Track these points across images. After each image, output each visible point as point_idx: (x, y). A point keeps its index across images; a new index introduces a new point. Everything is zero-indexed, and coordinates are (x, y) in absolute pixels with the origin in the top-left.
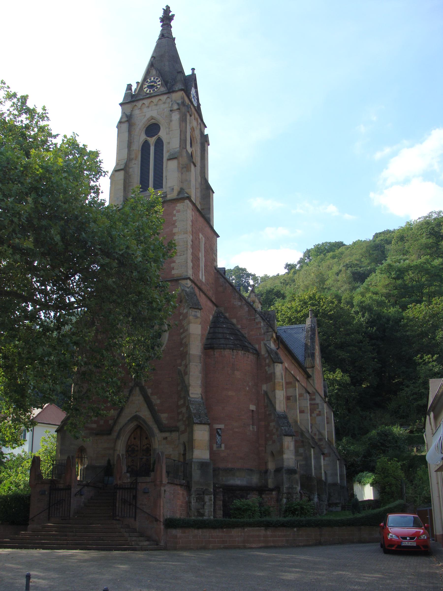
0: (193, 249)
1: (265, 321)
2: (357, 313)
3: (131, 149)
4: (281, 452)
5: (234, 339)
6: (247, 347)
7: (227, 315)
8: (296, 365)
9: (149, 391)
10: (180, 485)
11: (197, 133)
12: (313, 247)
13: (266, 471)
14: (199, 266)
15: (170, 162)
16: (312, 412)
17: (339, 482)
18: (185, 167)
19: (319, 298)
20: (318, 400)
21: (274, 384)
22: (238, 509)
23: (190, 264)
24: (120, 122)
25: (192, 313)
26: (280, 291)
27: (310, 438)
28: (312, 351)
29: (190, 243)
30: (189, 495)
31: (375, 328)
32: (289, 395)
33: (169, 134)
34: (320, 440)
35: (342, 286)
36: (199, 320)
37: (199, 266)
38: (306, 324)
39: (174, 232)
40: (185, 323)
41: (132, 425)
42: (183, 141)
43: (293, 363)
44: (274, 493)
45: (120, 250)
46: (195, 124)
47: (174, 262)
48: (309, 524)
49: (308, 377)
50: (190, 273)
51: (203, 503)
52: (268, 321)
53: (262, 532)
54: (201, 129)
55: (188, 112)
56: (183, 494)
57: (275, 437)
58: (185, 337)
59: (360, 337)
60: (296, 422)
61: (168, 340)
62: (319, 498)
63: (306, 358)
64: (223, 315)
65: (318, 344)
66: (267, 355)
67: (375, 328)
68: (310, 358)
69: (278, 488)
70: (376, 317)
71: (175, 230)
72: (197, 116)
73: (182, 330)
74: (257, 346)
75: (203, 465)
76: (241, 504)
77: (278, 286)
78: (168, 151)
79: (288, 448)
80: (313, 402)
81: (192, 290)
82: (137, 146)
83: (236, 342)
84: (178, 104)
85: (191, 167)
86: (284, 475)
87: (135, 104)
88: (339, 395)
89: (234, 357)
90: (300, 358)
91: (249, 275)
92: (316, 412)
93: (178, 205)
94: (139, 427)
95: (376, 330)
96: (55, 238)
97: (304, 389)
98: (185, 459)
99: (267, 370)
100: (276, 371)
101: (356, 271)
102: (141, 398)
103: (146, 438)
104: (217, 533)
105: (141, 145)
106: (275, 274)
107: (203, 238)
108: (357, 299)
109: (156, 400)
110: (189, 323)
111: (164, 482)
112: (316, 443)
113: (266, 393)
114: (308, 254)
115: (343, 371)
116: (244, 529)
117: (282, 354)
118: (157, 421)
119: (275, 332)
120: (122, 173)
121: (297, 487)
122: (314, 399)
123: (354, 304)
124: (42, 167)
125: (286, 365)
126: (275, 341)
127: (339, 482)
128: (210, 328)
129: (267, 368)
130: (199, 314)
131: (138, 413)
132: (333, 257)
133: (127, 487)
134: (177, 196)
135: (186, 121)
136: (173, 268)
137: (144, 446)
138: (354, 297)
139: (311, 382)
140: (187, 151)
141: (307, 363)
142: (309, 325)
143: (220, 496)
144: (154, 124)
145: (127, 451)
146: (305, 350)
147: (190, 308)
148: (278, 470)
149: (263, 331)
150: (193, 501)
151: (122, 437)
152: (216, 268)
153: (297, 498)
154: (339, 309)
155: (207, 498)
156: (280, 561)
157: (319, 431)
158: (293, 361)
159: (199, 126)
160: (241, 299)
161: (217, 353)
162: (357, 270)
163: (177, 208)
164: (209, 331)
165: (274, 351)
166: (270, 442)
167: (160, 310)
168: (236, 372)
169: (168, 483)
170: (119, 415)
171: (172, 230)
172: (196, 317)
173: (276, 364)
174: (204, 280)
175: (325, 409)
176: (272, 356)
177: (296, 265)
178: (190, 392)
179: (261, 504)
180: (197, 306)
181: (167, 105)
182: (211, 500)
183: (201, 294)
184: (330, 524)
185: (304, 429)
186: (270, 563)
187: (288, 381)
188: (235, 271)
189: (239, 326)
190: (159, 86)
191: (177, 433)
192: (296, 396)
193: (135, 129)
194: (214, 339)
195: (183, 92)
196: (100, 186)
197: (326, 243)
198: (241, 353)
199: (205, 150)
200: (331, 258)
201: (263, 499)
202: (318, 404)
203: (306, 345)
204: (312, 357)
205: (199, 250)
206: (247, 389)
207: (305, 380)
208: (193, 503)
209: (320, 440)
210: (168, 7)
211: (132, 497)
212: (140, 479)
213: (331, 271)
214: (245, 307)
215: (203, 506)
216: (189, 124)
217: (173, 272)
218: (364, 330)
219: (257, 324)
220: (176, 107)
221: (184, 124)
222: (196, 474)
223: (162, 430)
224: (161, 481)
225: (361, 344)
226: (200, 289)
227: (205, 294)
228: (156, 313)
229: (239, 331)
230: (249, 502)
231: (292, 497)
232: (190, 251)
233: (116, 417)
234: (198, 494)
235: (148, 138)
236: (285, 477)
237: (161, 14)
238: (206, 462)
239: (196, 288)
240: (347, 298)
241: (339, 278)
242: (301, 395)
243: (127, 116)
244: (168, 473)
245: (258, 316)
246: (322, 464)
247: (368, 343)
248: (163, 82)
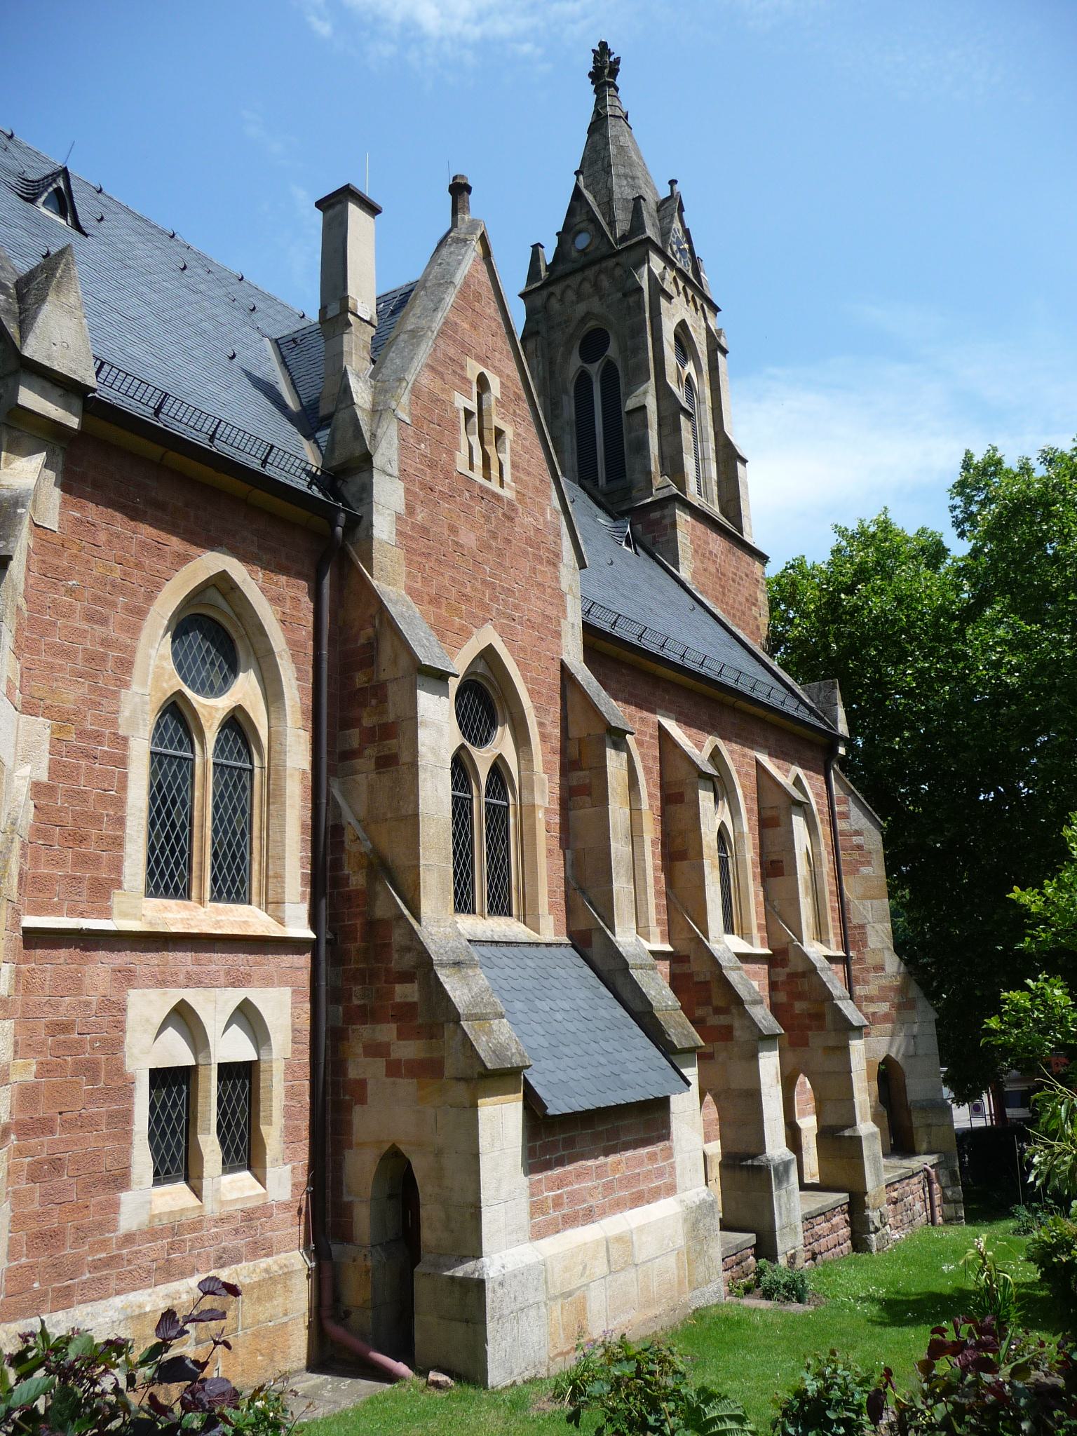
210: (603, 45)
235: (585, 365)
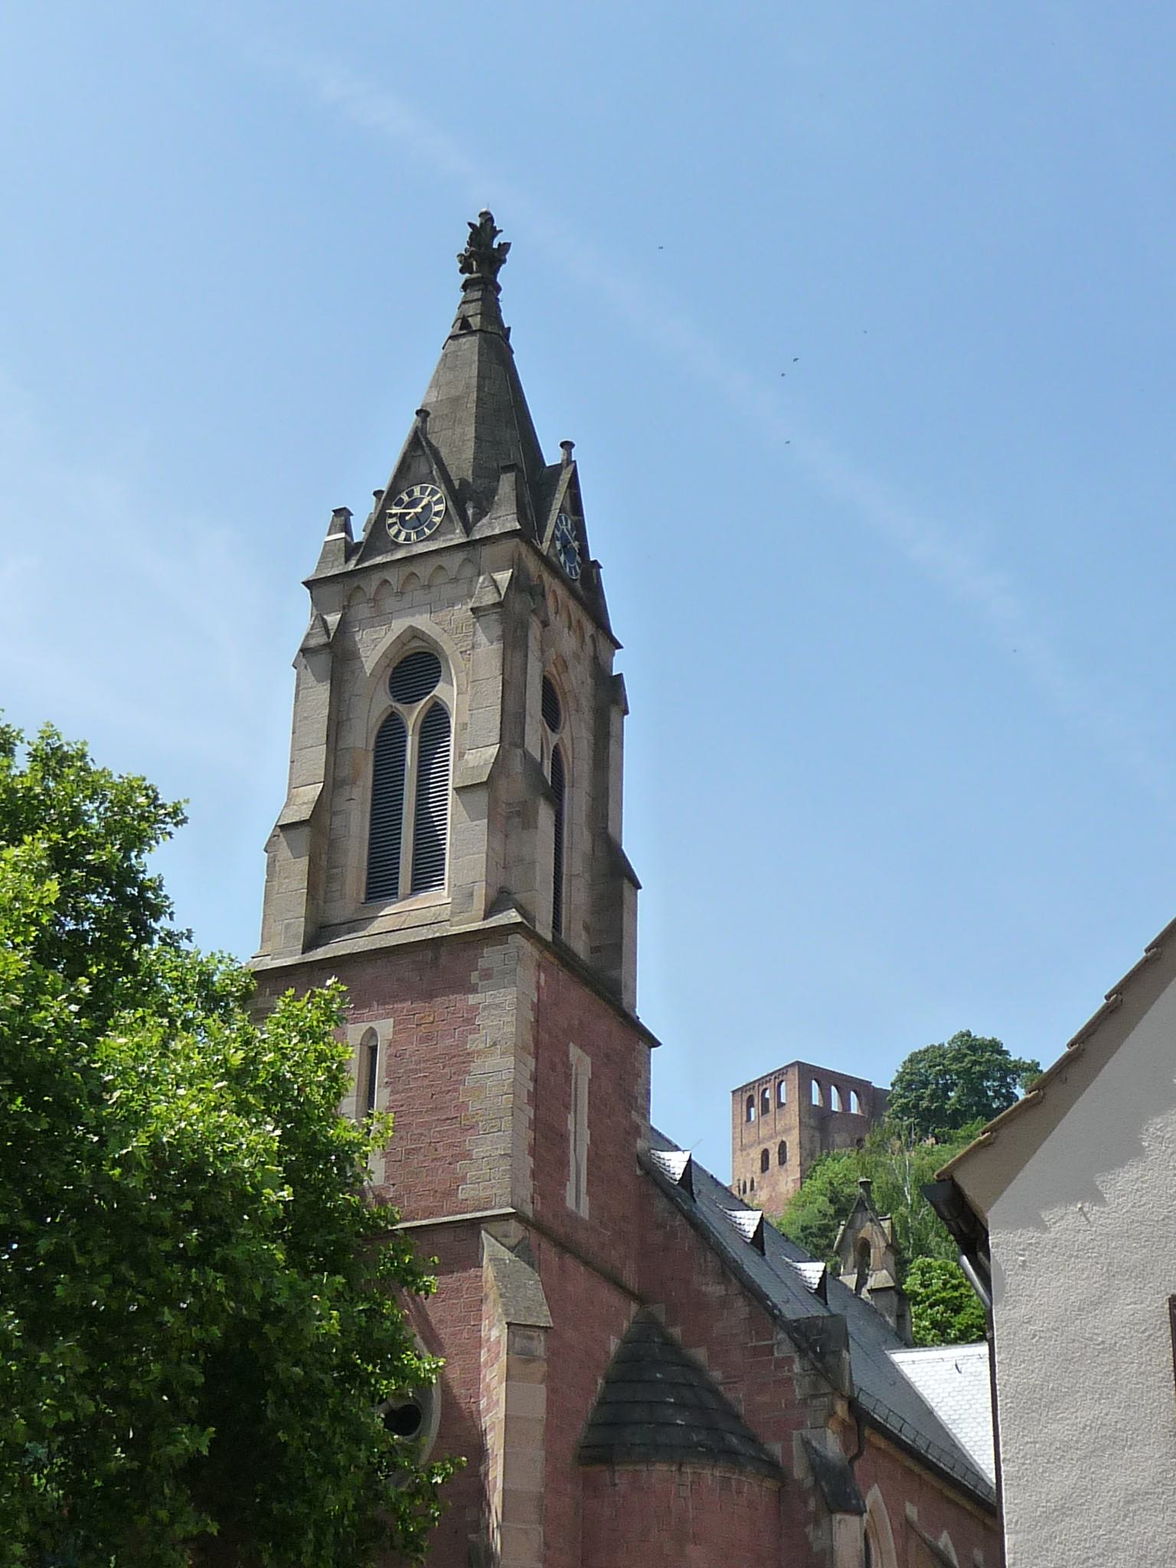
0: (536, 1108)
1: (806, 1355)
3: (341, 745)
5: (686, 1425)
7: (676, 1332)
11: (577, 681)
14: (563, 1163)
18: (518, 813)
43: (949, 1501)
46: (568, 643)
47: (467, 1155)
52: (821, 1357)
54: (595, 658)
74: (776, 1449)
82: (362, 736)
99: (811, 1538)
105: (375, 732)
125: (912, 1511)
135: (527, 647)
144: (419, 653)
149: (798, 1394)
160: (723, 1272)
161: (622, 1477)
163: (481, 963)
173: (838, 1517)
189: (717, 1375)
190: (437, 520)
195: (517, 540)
198: (712, 1475)
199: (608, 733)
210: (487, 217)
214: (740, 1303)
216: (538, 654)
221: (518, 659)
235: (398, 706)
237: (461, 242)
245: (782, 1336)
248: (450, 503)
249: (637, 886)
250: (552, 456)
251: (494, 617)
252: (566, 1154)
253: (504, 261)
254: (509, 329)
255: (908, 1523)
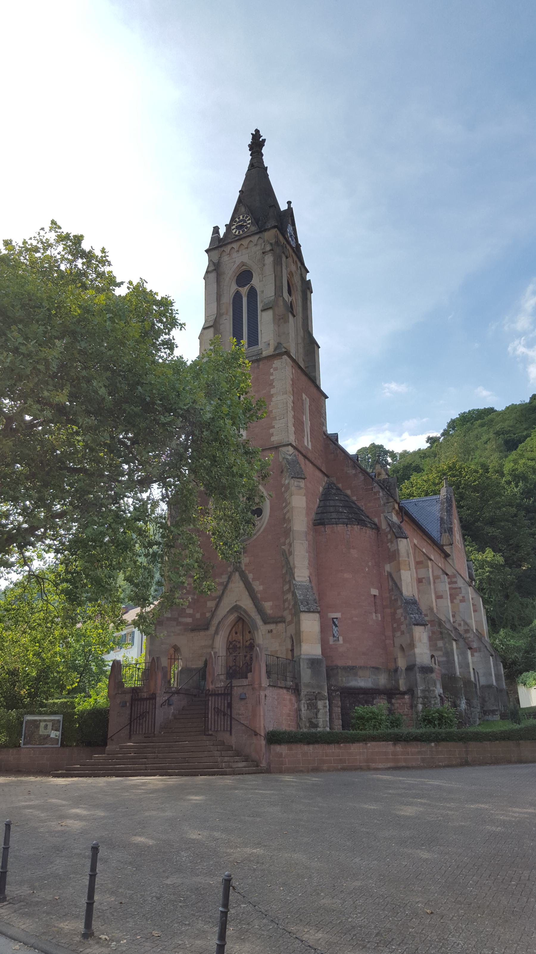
0: (294, 412)
2: (509, 483)
3: (221, 302)
4: (412, 646)
6: (364, 521)
7: (340, 486)
8: (429, 542)
9: (250, 576)
10: (285, 688)
11: (297, 279)
12: (458, 416)
13: (396, 670)
14: (303, 431)
15: (265, 314)
16: (453, 598)
17: (494, 683)
18: (282, 318)
19: (461, 468)
20: (460, 583)
21: (399, 563)
22: (361, 718)
23: (292, 429)
24: (207, 272)
25: (294, 483)
26: (419, 466)
27: (452, 629)
28: (449, 526)
29: (290, 405)
30: (299, 700)
31: (532, 499)
32: (420, 576)
33: (262, 281)
34: (467, 631)
35: (491, 455)
36: (303, 491)
37: (304, 431)
38: (441, 495)
39: (272, 393)
40: (287, 495)
41: (232, 618)
42: (278, 289)
44: (406, 697)
45: (185, 405)
46: (293, 268)
47: (273, 427)
48: (449, 738)
49: (447, 556)
50: (292, 439)
51: (315, 710)
53: (389, 747)
54: (301, 275)
55: (284, 253)
56: (291, 700)
57: (403, 627)
58: (288, 511)
59: (514, 510)
60: (431, 609)
61: (270, 516)
62: (469, 703)
63: (441, 534)
64: (335, 486)
65: (457, 518)
66: (388, 529)
67: (532, 499)
68: (447, 534)
69: (411, 691)
70: (532, 486)
71: (273, 391)
72: (295, 258)
73: (284, 504)
74: (376, 520)
75: (314, 663)
76: (364, 712)
77: (418, 461)
78: (262, 301)
79: (420, 640)
80: (454, 586)
81: (294, 458)
83: (350, 516)
84: (271, 244)
85: (289, 317)
86: (418, 674)
87: (222, 249)
88: (491, 578)
89: (349, 533)
90: (435, 534)
91: (386, 452)
92: (459, 597)
93: (275, 362)
94: (240, 619)
95: (533, 502)
96: (99, 392)
97: (441, 571)
98: (293, 655)
99: (390, 547)
100: (400, 548)
101: (509, 438)
102: (241, 585)
103: (250, 632)
104: (332, 749)
106: (417, 449)
107: (308, 400)
108: (508, 466)
109: (258, 587)
110: (291, 495)
111: (263, 685)
112: (461, 635)
113: (390, 575)
114: (453, 424)
115: (494, 551)
116: (366, 744)
117: (407, 528)
118: (260, 611)
119: (397, 503)
120: (211, 330)
121: (434, 688)
122: (456, 582)
123: (505, 472)
124: (80, 307)
125: (415, 541)
126: (397, 514)
127: (494, 683)
128: (320, 501)
129: (389, 544)
130: (302, 483)
131: (238, 603)
132: (482, 425)
133: (220, 692)
134: (274, 351)
136: (272, 435)
137: (247, 641)
138: (504, 465)
139: (450, 561)
140: (283, 298)
141: (444, 540)
142: (444, 496)
143: (338, 702)
145: (228, 649)
146: (441, 525)
147: (292, 477)
148: (410, 668)
149: (382, 502)
150: (304, 709)
151: (221, 632)
152: (325, 433)
153: (436, 704)
154: (485, 478)
155: (320, 704)
156: (404, 788)
157: (464, 621)
158: (424, 537)
159: (299, 270)
160: (355, 466)
161: (328, 529)
162: (510, 437)
163: (274, 366)
164: (319, 505)
165: (396, 524)
166: (398, 634)
167: (241, 476)
168: (352, 550)
169: (269, 686)
170: (217, 606)
171: (270, 392)
172: (299, 487)
173: (399, 539)
174: (310, 447)
175: (471, 593)
176: (395, 531)
177: (440, 438)
178: (296, 575)
179: (391, 711)
180: (299, 476)
181: (258, 247)
182: (326, 707)
183: (307, 462)
184: (478, 737)
185: (443, 618)
186: (390, 791)
187: (418, 560)
188: (371, 448)
189: (354, 498)
191: (284, 624)
192: (429, 578)
193: (224, 278)
194: (324, 513)
195: (276, 229)
196: (174, 339)
197: (474, 410)
198: (356, 528)
200: (479, 426)
201: (392, 704)
202: (460, 588)
203: (442, 519)
204: (449, 533)
205: (303, 413)
206: (367, 570)
207: (443, 560)
208: (303, 711)
209: (467, 631)
210: (257, 131)
211: (226, 705)
212: (235, 682)
213: (480, 441)
214: (361, 475)
215: (316, 715)
217: (273, 439)
218: (518, 501)
219: (375, 494)
220: (268, 248)
222: (306, 675)
223: (265, 622)
224: (260, 684)
225: (515, 518)
226: (305, 457)
227: (312, 463)
228: (237, 479)
229: (355, 504)
230: (374, 709)
231: (430, 702)
232: (291, 414)
233: (213, 609)
234: (309, 699)
236: (419, 676)
238: (318, 659)
239: (300, 455)
240: (495, 466)
241: (488, 446)
242: (436, 578)
243: (214, 264)
244: (269, 673)
245: (375, 484)
246: (470, 660)
247: (524, 516)
248: (253, 219)
249: (319, 347)
250: (283, 207)
251: (270, 254)
252: (304, 428)
253: (264, 145)
254: (267, 167)
255: (415, 544)
